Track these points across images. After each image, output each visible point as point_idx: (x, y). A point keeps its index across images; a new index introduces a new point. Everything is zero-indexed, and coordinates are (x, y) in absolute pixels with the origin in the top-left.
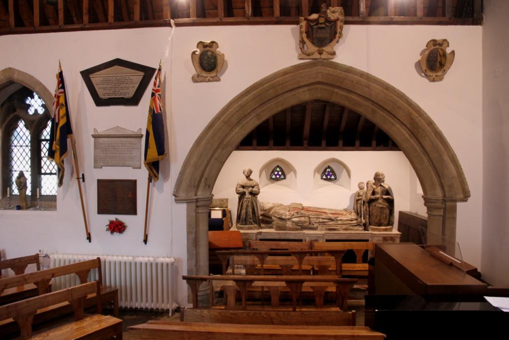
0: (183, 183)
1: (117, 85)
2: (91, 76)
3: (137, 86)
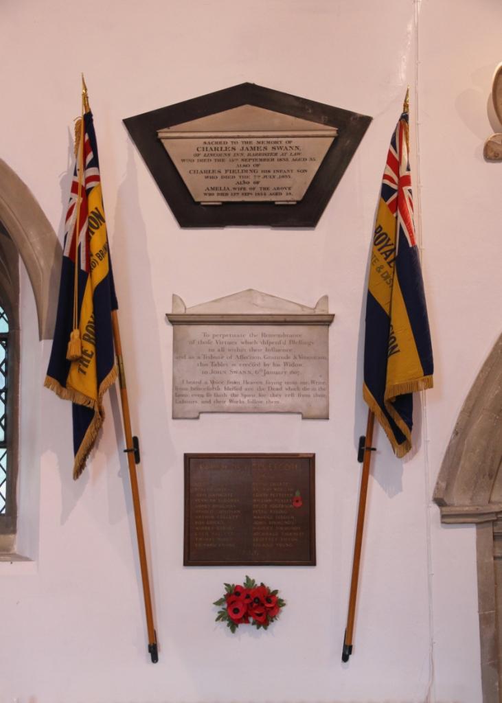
0: (462, 462)
1: (252, 163)
2: (162, 134)
3: (314, 167)
